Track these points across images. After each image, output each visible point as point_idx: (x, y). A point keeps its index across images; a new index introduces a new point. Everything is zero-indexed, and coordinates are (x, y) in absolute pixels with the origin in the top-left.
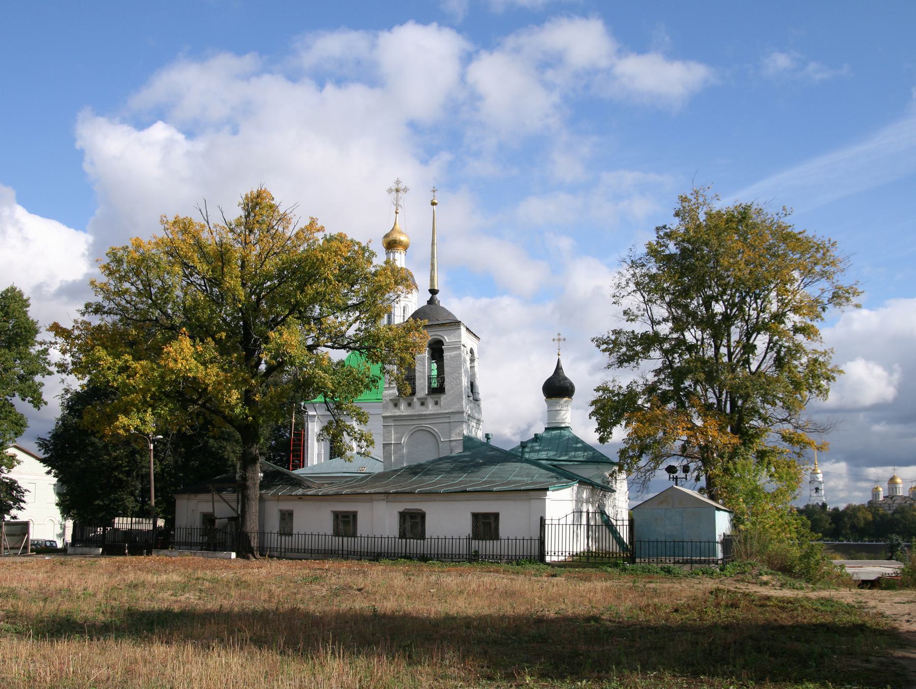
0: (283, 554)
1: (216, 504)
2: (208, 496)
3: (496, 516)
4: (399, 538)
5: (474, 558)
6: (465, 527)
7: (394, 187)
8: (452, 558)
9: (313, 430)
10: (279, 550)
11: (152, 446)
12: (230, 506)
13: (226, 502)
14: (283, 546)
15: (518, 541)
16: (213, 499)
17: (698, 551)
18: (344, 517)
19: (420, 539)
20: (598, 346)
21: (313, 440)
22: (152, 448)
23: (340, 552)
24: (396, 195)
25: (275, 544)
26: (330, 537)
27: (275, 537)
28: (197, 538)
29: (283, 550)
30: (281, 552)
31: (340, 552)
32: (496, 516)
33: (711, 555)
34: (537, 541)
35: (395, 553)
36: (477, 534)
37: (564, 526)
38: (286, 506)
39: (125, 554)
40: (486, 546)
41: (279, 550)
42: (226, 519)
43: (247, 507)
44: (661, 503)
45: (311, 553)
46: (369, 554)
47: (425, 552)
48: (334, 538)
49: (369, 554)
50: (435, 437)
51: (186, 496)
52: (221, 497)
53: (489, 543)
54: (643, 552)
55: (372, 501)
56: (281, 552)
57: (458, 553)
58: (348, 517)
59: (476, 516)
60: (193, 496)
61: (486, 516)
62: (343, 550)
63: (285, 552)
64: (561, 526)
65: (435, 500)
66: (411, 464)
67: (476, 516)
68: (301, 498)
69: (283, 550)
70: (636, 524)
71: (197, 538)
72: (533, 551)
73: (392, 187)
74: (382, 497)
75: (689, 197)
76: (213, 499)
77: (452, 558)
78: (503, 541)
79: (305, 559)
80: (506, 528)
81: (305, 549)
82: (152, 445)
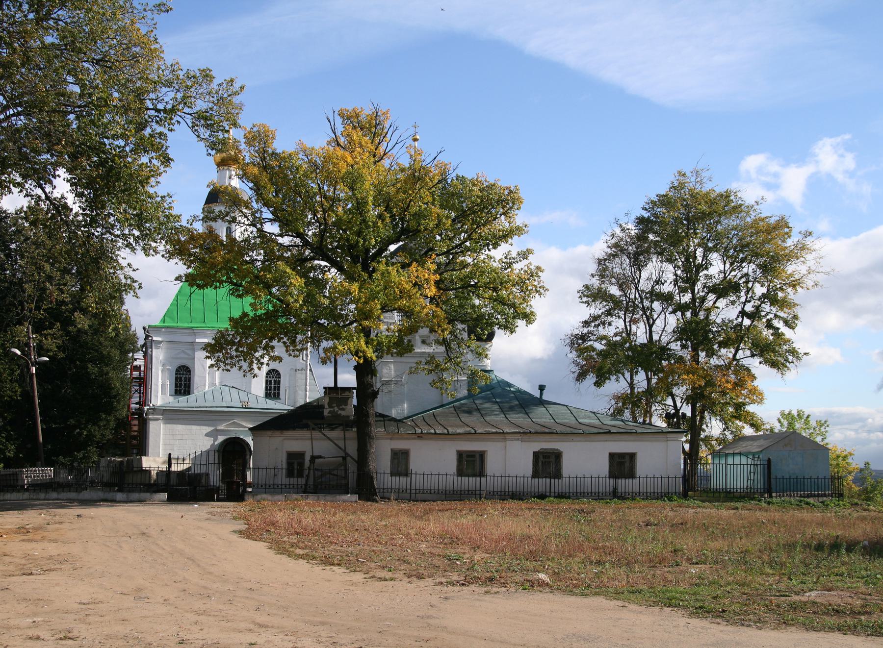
0: (413, 495)
1: (347, 441)
2: (306, 434)
3: (632, 456)
4: (609, 477)
5: (615, 494)
6: (602, 467)
9: (157, 358)
11: (34, 370)
12: (336, 445)
13: (331, 440)
15: (649, 479)
17: (816, 487)
18: (468, 456)
19: (629, 478)
20: (580, 297)
21: (157, 369)
22: (34, 372)
23: (478, 492)
25: (388, 485)
27: (388, 478)
30: (410, 493)
31: (478, 492)
32: (632, 456)
34: (681, 479)
36: (613, 475)
37: (745, 466)
39: (214, 501)
40: (625, 485)
41: (409, 491)
42: (341, 459)
43: (368, 445)
44: (786, 445)
47: (564, 491)
51: (269, 433)
52: (324, 435)
53: (629, 481)
54: (806, 487)
55: (505, 440)
56: (410, 493)
57: (638, 491)
58: (473, 456)
60: (277, 433)
61: (622, 455)
62: (411, 489)
64: (735, 466)
65: (573, 441)
66: (835, 409)
67: (612, 456)
68: (420, 436)
69: (413, 491)
70: (772, 464)
74: (518, 436)
75: (688, 174)
78: (564, 479)
80: (642, 467)
82: (34, 368)
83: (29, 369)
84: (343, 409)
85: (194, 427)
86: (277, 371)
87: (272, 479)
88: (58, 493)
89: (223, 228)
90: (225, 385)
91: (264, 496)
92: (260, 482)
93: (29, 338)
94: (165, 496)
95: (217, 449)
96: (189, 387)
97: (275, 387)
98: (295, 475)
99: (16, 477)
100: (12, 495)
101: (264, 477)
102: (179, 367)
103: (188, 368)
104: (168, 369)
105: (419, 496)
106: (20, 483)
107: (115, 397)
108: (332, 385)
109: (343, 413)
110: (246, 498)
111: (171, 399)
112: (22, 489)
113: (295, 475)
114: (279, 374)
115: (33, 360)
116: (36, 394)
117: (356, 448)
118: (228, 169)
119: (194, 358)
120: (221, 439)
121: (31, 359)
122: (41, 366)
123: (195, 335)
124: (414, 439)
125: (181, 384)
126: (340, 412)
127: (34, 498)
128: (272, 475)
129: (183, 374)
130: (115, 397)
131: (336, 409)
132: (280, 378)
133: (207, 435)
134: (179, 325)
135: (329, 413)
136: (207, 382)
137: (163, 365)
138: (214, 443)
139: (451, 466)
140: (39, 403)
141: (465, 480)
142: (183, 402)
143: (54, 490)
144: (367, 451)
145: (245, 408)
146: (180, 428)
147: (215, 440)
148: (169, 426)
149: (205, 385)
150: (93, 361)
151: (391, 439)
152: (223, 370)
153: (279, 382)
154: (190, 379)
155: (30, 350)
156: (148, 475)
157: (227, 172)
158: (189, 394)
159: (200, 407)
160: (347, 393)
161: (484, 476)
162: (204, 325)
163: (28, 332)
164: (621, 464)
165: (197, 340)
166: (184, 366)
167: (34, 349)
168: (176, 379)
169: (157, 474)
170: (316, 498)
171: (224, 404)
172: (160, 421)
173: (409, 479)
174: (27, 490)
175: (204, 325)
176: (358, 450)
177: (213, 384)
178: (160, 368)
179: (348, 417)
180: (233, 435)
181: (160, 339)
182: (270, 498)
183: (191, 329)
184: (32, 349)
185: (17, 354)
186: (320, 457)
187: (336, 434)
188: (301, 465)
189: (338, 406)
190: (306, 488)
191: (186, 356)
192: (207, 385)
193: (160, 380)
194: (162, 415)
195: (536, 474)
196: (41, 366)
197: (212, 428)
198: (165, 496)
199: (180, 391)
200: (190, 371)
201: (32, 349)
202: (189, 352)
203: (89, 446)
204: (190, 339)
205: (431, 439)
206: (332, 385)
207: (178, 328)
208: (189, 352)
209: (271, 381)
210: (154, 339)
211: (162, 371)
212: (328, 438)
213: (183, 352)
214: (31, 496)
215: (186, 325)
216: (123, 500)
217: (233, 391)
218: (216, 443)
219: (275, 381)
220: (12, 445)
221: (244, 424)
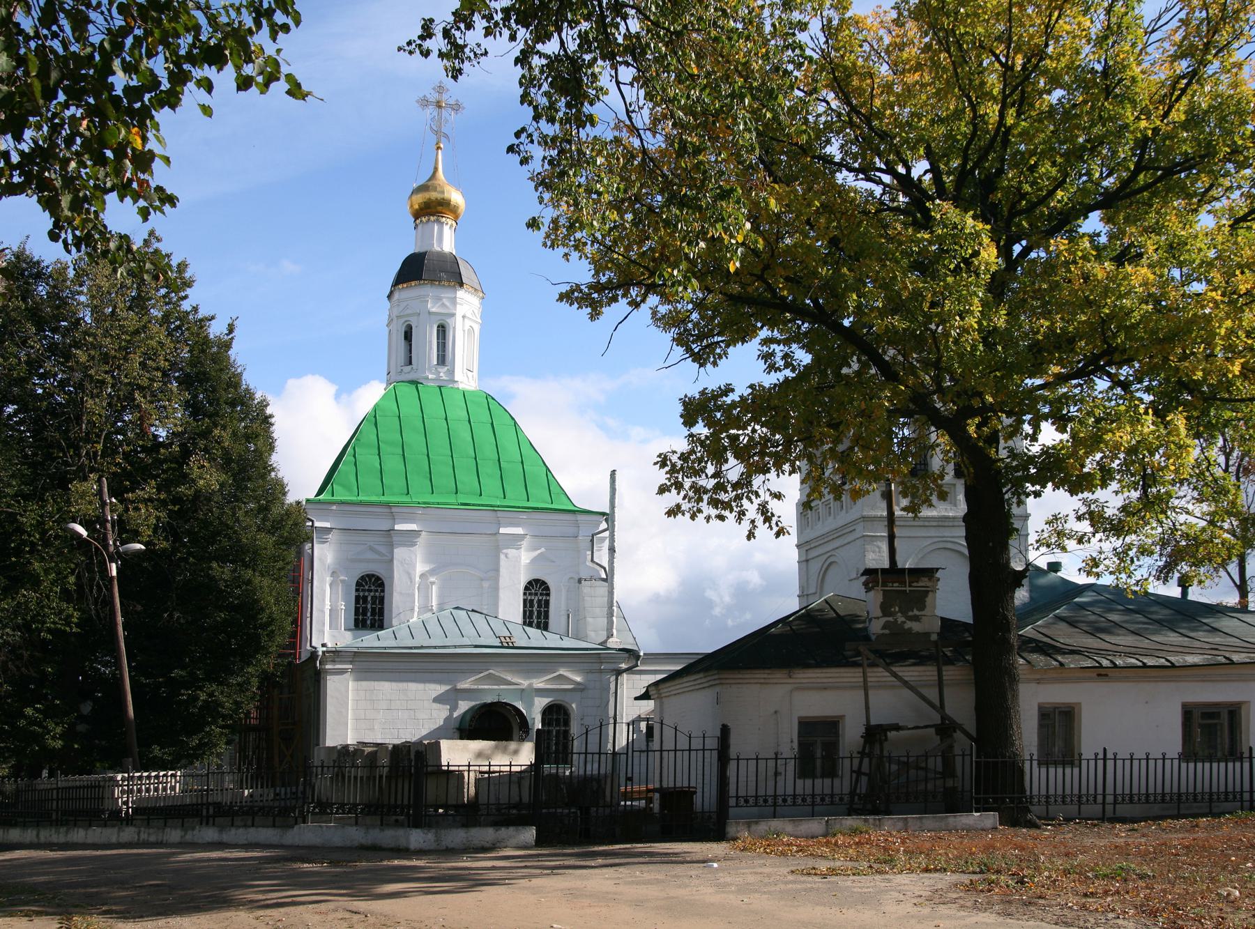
0: (1109, 808)
1: (871, 693)
2: (850, 675)
7: (433, 97)
8: (813, 804)
10: (1100, 798)
11: (114, 570)
13: (911, 688)
14: (1110, 790)
16: (865, 681)
18: (1206, 715)
21: (322, 581)
22: (114, 573)
24: (435, 113)
26: (1176, 762)
28: (789, 783)
29: (1110, 799)
33: (486, 782)
35: (1179, 795)
38: (1058, 694)
41: (1100, 798)
42: (932, 730)
45: (775, 805)
46: (837, 799)
48: (1184, 765)
49: (837, 799)
50: (827, 569)
59: (1188, 712)
60: (779, 675)
63: (1115, 802)
69: (1110, 799)
71: (789, 783)
72: (762, 784)
73: (428, 96)
76: (865, 681)
77: (813, 804)
79: (1228, 813)
81: (1064, 797)
82: (114, 566)
83: (104, 571)
84: (916, 619)
85: (413, 686)
86: (544, 583)
87: (771, 783)
88: (221, 831)
89: (431, 327)
90: (457, 608)
91: (776, 824)
92: (762, 793)
93: (103, 504)
94: (530, 834)
95: (457, 725)
96: (381, 612)
97: (539, 613)
98: (819, 771)
99: (102, 790)
100: (90, 832)
101: (752, 778)
102: (363, 578)
103: (378, 578)
104: (342, 581)
105: (1122, 810)
106: (107, 804)
107: (264, 626)
108: (886, 565)
109: (916, 627)
110: (731, 830)
111: (349, 635)
112: (115, 818)
113: (819, 771)
114: (547, 588)
115: (112, 549)
116: (120, 619)
117: (974, 705)
118: (438, 221)
119: (391, 561)
120: (464, 706)
121: (106, 546)
122: (129, 563)
123: (393, 518)
124: (1090, 679)
125: (365, 610)
126: (909, 625)
127: (152, 839)
128: (771, 772)
129: (370, 591)
130: (264, 626)
131: (901, 619)
132: (548, 595)
133: (437, 700)
134: (360, 498)
135: (884, 627)
136: (416, 604)
137: (333, 574)
138: (451, 714)
139: (1171, 740)
140: (125, 638)
141: (1203, 768)
142: (370, 640)
143: (207, 821)
144: (1008, 709)
145: (509, 647)
146: (386, 689)
147: (453, 709)
148: (365, 684)
149: (412, 610)
150: (222, 558)
151: (1039, 681)
152: (708, 518)
153: (547, 603)
154: (382, 600)
155: (105, 529)
156: (453, 782)
157: (436, 227)
158: (381, 627)
159: (422, 647)
160: (924, 582)
161: (1072, 764)
162: (406, 499)
163: (100, 492)
164: (1210, 732)
165: (397, 527)
166: (370, 576)
167: (113, 527)
168: (357, 598)
169: (477, 781)
170: (900, 824)
171: (466, 641)
172: (347, 675)
173: (1076, 770)
174: (129, 821)
175: (406, 499)
176: (977, 708)
177: (426, 608)
178: (328, 579)
179: (927, 634)
180: (489, 700)
181: (328, 525)
182: (789, 827)
183: (387, 505)
184: (109, 526)
185: (80, 535)
186: (897, 728)
187: (910, 673)
188: (832, 747)
189: (904, 612)
190: (852, 801)
191: (377, 557)
192: (416, 609)
193: (328, 602)
194: (351, 662)
195: (1188, 755)
196: (129, 563)
197: (448, 687)
198: (530, 834)
199: (364, 621)
200: (382, 585)
201: (109, 526)
202: (382, 549)
203: (209, 724)
204: (385, 525)
205: (1126, 679)
206: (886, 565)
207: (361, 504)
208: (382, 549)
209: (531, 601)
210: (317, 524)
211: (331, 585)
212: (906, 684)
213: (371, 549)
214: (144, 836)
215: (374, 498)
216: (425, 846)
217: (474, 616)
218: (455, 715)
219: (539, 601)
220: (57, 724)
221: (509, 678)
